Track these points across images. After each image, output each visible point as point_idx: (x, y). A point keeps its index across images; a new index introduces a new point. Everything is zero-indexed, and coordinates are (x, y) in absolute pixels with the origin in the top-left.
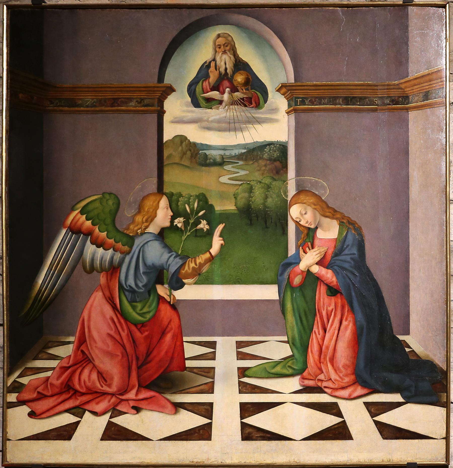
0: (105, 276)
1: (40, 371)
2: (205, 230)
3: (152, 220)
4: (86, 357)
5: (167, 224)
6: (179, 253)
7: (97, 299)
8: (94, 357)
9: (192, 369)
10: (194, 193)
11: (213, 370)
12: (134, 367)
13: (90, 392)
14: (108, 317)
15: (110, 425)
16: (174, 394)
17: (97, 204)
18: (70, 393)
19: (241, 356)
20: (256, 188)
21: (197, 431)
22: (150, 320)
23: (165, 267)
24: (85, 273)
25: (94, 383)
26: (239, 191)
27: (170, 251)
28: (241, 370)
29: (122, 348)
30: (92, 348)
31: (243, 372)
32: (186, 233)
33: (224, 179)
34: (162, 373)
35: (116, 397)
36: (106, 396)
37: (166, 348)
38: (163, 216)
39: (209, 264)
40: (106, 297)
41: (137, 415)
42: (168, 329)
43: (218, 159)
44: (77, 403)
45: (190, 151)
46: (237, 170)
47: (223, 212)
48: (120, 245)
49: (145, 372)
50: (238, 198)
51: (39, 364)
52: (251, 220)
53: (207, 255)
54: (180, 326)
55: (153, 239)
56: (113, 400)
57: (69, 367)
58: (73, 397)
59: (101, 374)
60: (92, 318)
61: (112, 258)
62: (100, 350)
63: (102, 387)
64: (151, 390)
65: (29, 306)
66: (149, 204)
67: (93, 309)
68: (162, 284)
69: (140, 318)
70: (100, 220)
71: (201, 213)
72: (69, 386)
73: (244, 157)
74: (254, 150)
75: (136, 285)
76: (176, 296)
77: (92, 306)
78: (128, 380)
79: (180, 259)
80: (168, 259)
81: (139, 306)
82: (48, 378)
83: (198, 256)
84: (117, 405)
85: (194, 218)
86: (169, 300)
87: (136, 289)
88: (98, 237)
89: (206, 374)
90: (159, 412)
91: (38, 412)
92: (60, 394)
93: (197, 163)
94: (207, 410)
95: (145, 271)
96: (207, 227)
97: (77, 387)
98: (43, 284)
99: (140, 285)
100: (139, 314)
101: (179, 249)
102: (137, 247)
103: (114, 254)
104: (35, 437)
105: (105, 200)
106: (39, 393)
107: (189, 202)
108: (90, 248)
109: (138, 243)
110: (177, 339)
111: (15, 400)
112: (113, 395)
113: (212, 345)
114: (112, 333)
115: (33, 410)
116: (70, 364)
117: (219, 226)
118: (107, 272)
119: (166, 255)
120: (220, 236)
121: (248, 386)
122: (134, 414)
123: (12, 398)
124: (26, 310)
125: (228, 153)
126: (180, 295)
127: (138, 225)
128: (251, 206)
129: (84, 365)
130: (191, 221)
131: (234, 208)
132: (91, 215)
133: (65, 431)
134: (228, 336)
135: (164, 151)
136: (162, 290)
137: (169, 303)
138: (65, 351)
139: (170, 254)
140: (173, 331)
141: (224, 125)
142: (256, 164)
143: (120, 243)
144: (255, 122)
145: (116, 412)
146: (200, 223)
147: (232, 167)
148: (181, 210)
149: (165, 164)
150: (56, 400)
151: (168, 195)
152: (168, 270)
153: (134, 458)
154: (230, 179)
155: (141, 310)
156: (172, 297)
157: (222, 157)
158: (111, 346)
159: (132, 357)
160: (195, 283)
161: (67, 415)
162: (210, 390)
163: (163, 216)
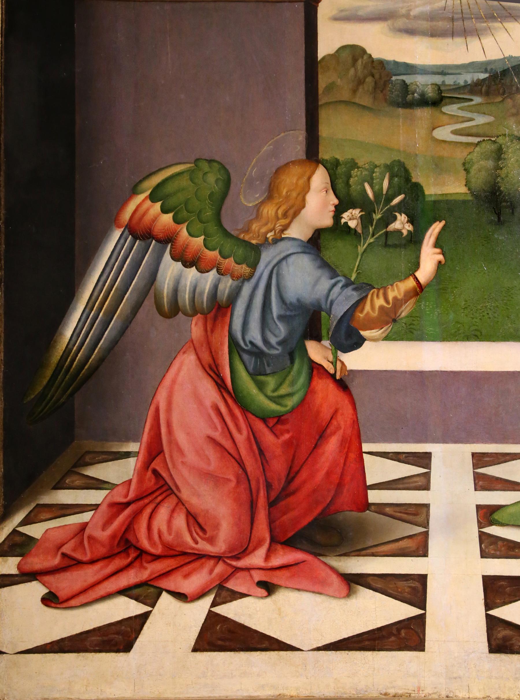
0: (201, 324)
1: (68, 511)
2: (405, 233)
3: (296, 214)
4: (161, 483)
5: (327, 221)
6: (353, 279)
7: (185, 368)
8: (179, 483)
9: (381, 508)
10: (382, 160)
11: (424, 510)
12: (262, 502)
13: (172, 553)
14: (208, 403)
15: (213, 620)
16: (346, 558)
17: (185, 182)
18: (128, 555)
19: (483, 483)
20: (510, 151)
21: (395, 632)
22: (293, 410)
23: (323, 306)
24: (161, 318)
25: (178, 535)
26: (475, 156)
27: (334, 274)
28: (485, 510)
29: (236, 464)
30: (174, 465)
31: (487, 514)
32: (365, 239)
33: (444, 133)
34: (320, 514)
35: (225, 562)
36: (203, 560)
37: (327, 465)
38: (318, 207)
39: (413, 300)
40: (204, 364)
41: (269, 600)
42: (332, 428)
43: (430, 93)
44: (144, 575)
45: (373, 76)
46: (469, 115)
47: (440, 198)
48: (230, 262)
49: (284, 514)
50: (473, 172)
51: (66, 497)
52: (499, 215)
53: (410, 283)
54: (356, 422)
55: (299, 250)
56: (220, 568)
57: (127, 504)
58: (137, 564)
59: (192, 518)
60: (174, 405)
61: (215, 287)
62: (192, 468)
63: (197, 543)
64: (297, 548)
65: (45, 382)
66: (290, 180)
67: (177, 387)
68: (318, 338)
69: (273, 406)
70: (188, 211)
71: (397, 200)
72: (127, 541)
73: (484, 89)
74: (505, 72)
75: (266, 341)
76: (346, 363)
77: (174, 382)
78: (249, 528)
79: (355, 289)
80: (330, 290)
81: (271, 382)
82: (84, 526)
83: (392, 285)
84: (227, 580)
85: (382, 212)
86: (332, 371)
87: (265, 349)
88: (186, 247)
89: (410, 518)
90: (313, 592)
91: (62, 594)
92: (109, 557)
93: (386, 100)
94: (414, 591)
95: (282, 312)
96: (409, 227)
97: (145, 544)
98: (74, 339)
99: (273, 340)
100: (270, 398)
101: (353, 270)
102: (266, 266)
103: (219, 281)
104: (56, 647)
105: (200, 175)
106: (64, 555)
107: (372, 179)
108: (170, 269)
109: (268, 260)
110: (348, 448)
111: (14, 571)
112: (218, 558)
113: (427, 456)
114: (217, 435)
115: (52, 591)
116: (129, 498)
117: (433, 226)
118: (205, 315)
119: (325, 283)
120: (436, 245)
121: (500, 543)
122: (262, 598)
123: (9, 566)
124: (39, 389)
125: (449, 80)
126: (354, 360)
127: (266, 224)
128: (499, 187)
129: (160, 498)
130: (377, 216)
131: (463, 190)
132: (172, 202)
133: (118, 633)
134: (456, 442)
135: (320, 76)
136: (317, 352)
137: (333, 376)
138: (120, 472)
139: (333, 281)
140: (342, 431)
141: (440, 24)
142: (509, 102)
143: (232, 259)
144: (506, 17)
145: (224, 593)
146: (395, 219)
147: (459, 108)
148: (354, 194)
149: (320, 103)
150: (102, 568)
151: (328, 165)
152: (329, 313)
153: (263, 686)
154: (455, 132)
155: (275, 390)
156: (339, 365)
157: (439, 88)
158: (213, 460)
159: (258, 482)
160: (387, 338)
161: (123, 601)
162: (421, 550)
163: (318, 207)
